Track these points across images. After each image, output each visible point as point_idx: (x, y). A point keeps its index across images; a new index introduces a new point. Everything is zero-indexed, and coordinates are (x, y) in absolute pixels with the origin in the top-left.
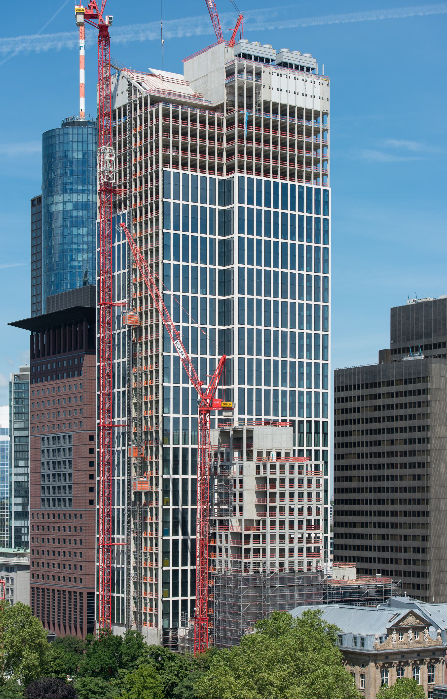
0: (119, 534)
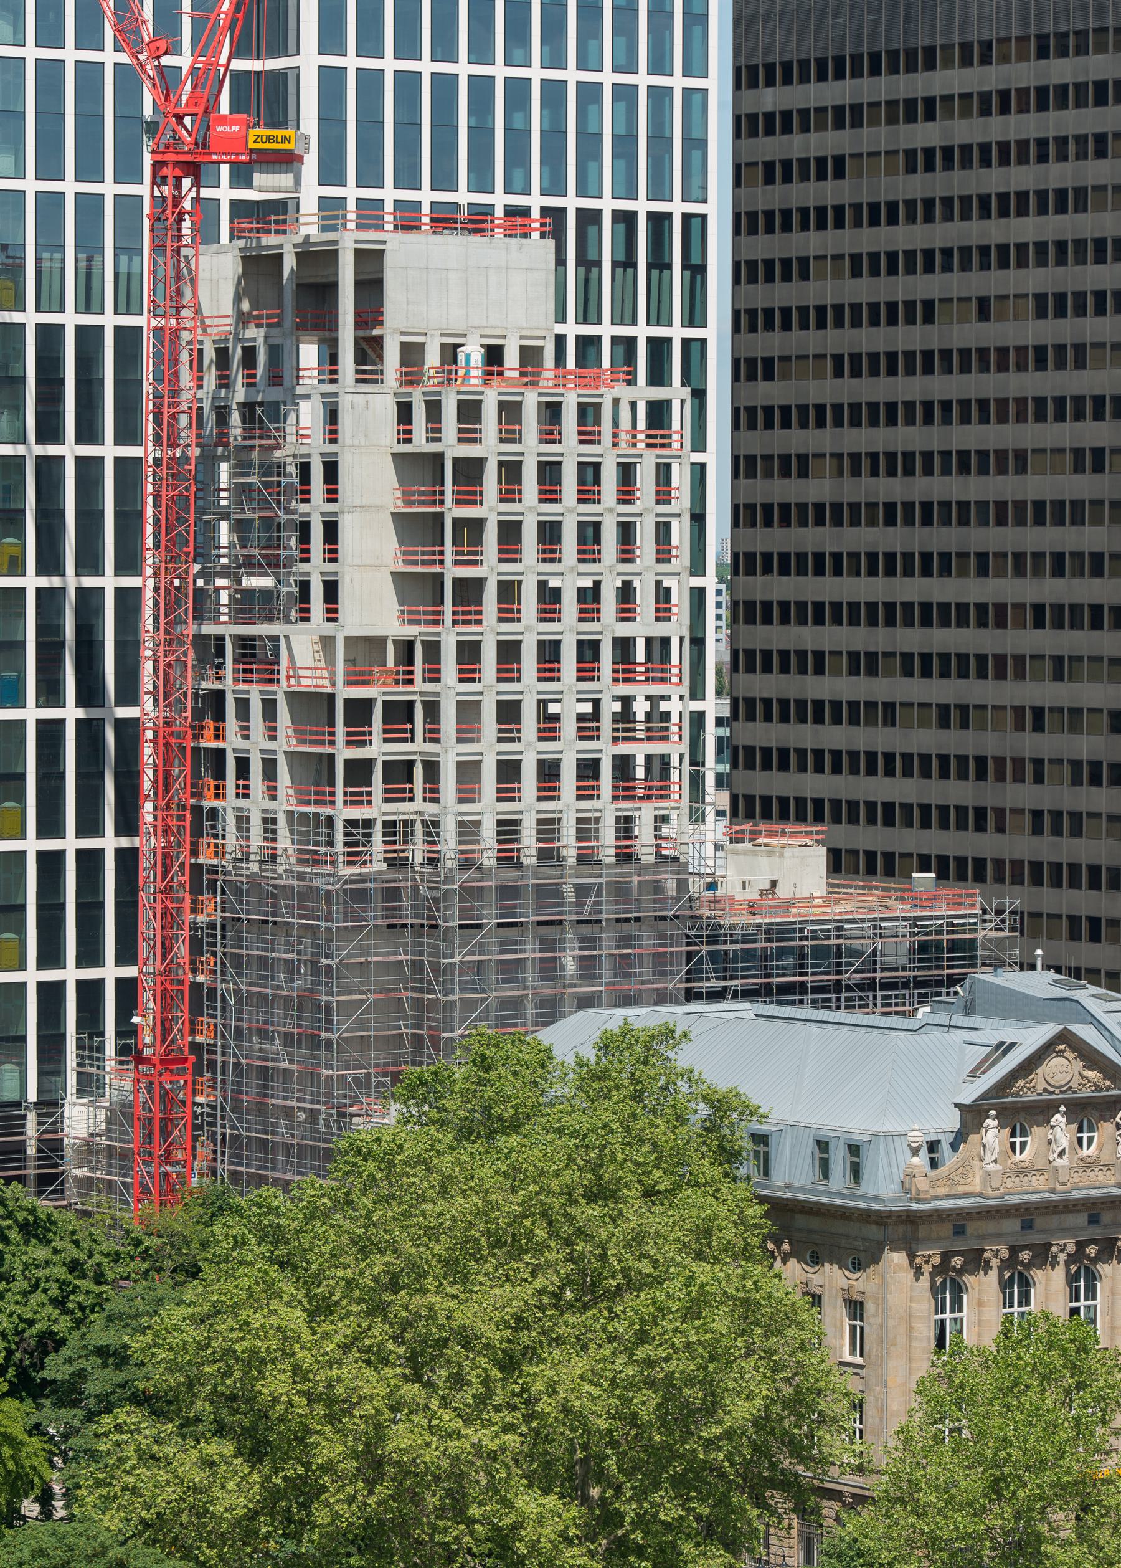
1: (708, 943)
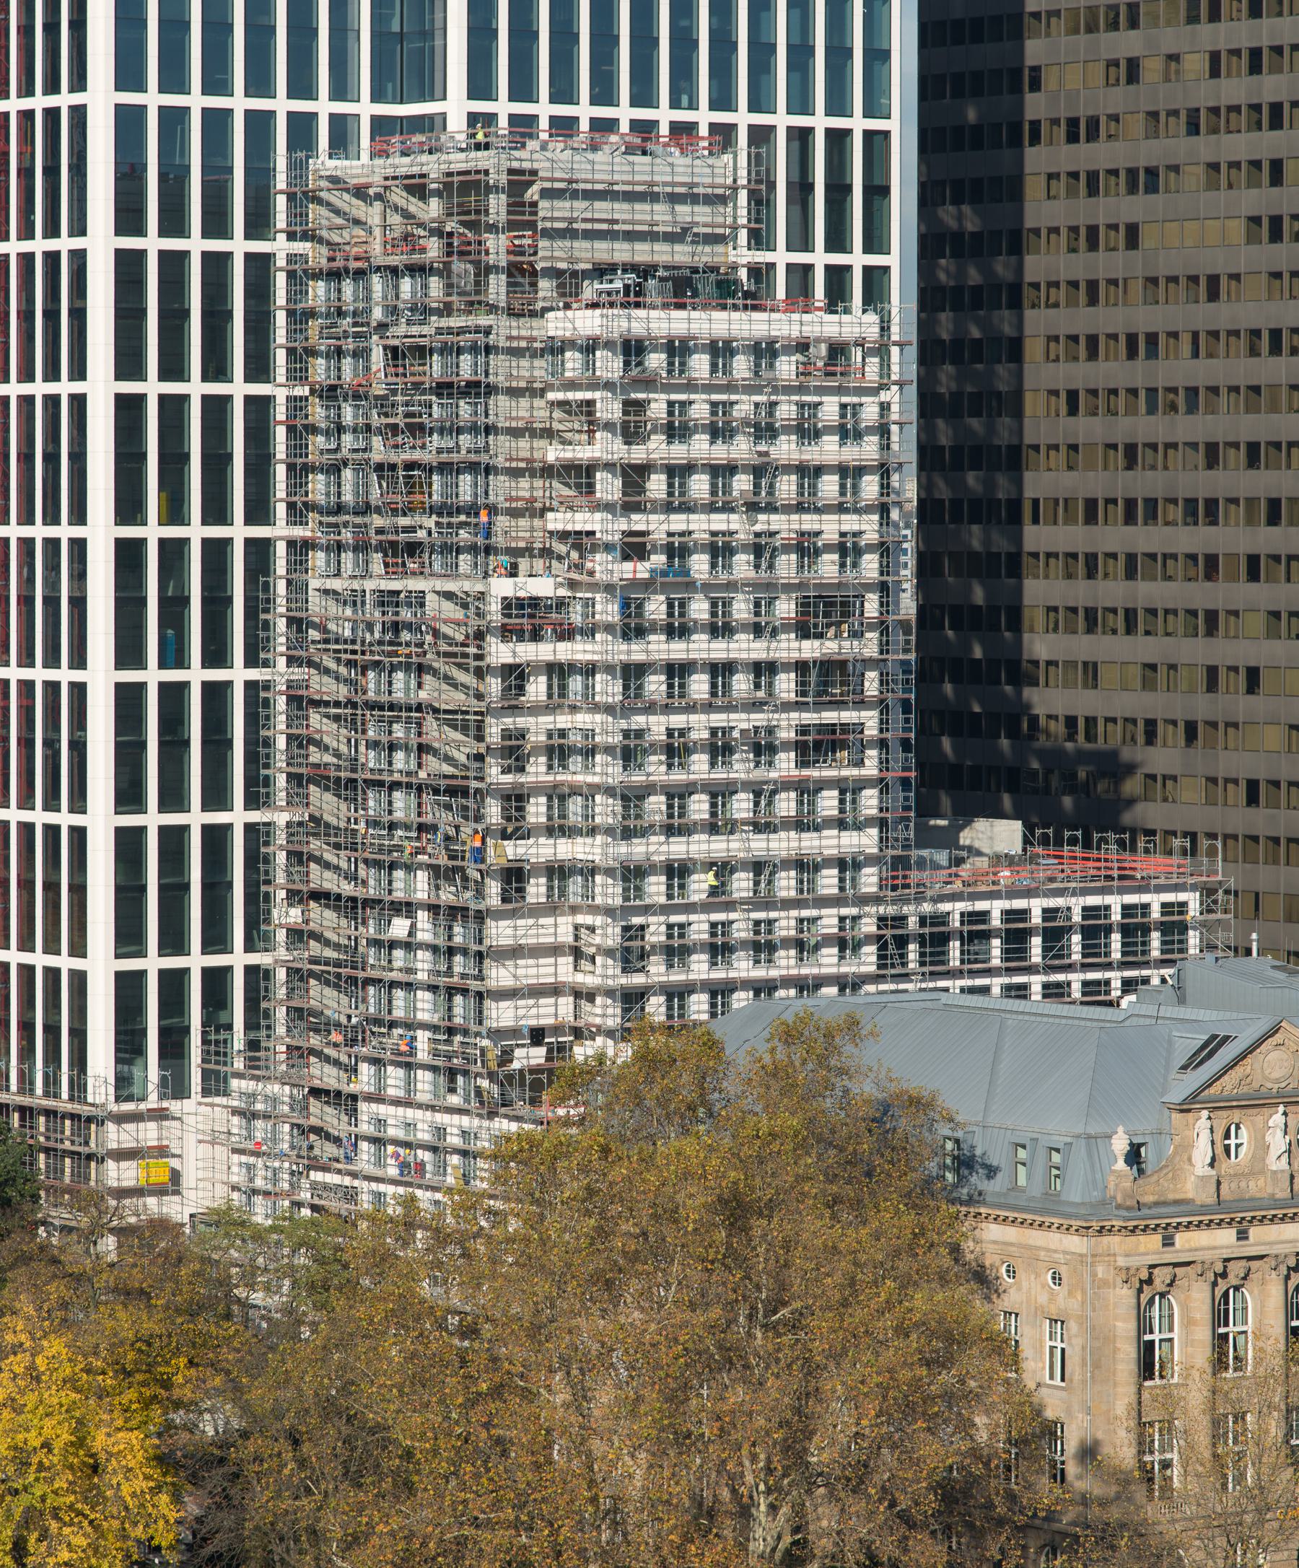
0: (56, 378)
1: (893, 927)
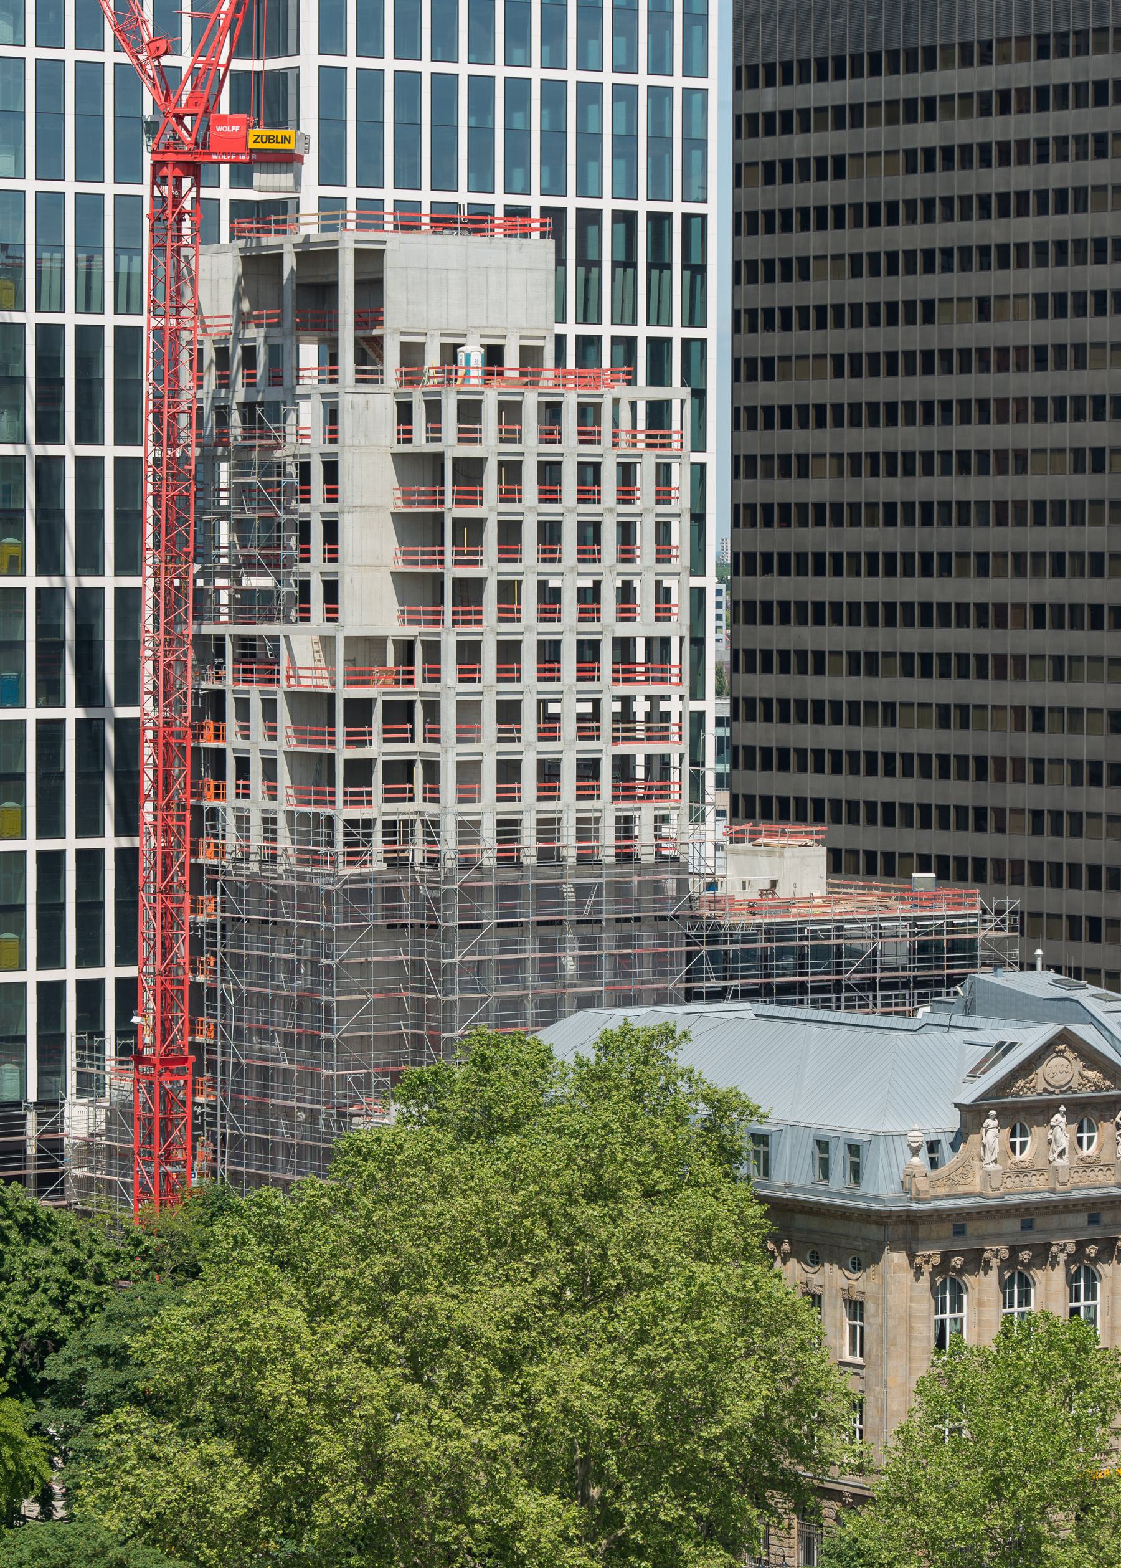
1: (708, 943)
